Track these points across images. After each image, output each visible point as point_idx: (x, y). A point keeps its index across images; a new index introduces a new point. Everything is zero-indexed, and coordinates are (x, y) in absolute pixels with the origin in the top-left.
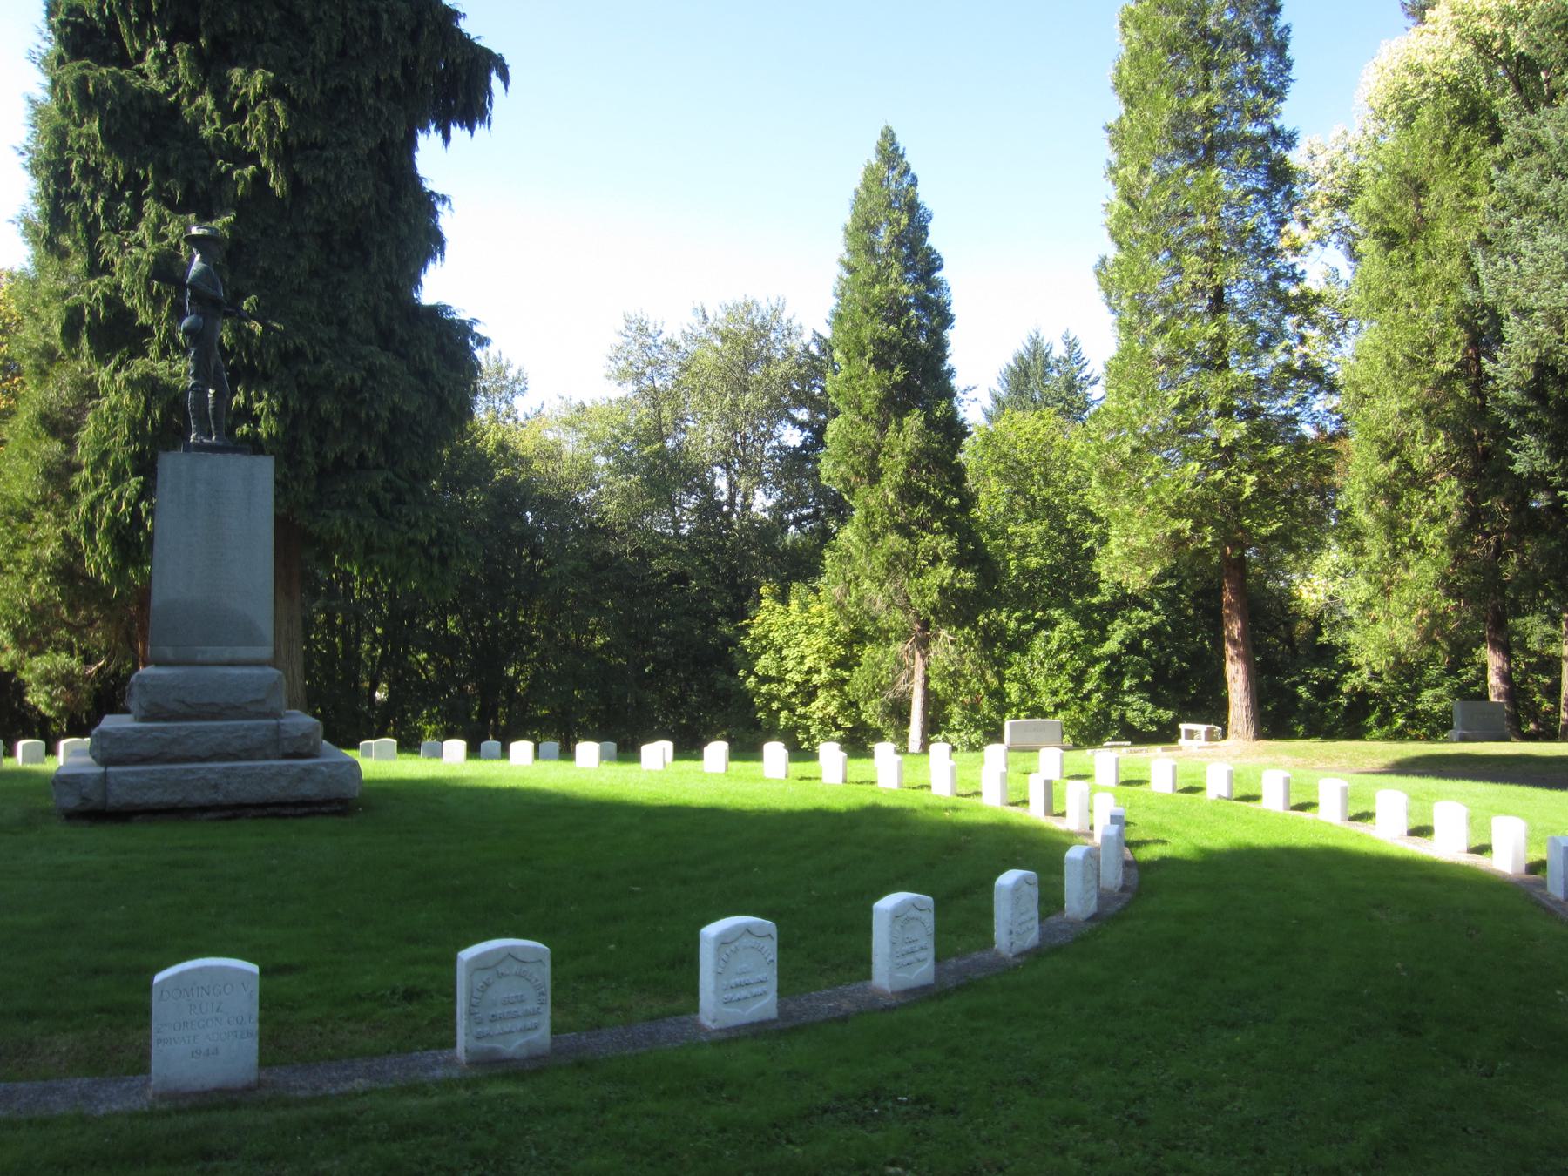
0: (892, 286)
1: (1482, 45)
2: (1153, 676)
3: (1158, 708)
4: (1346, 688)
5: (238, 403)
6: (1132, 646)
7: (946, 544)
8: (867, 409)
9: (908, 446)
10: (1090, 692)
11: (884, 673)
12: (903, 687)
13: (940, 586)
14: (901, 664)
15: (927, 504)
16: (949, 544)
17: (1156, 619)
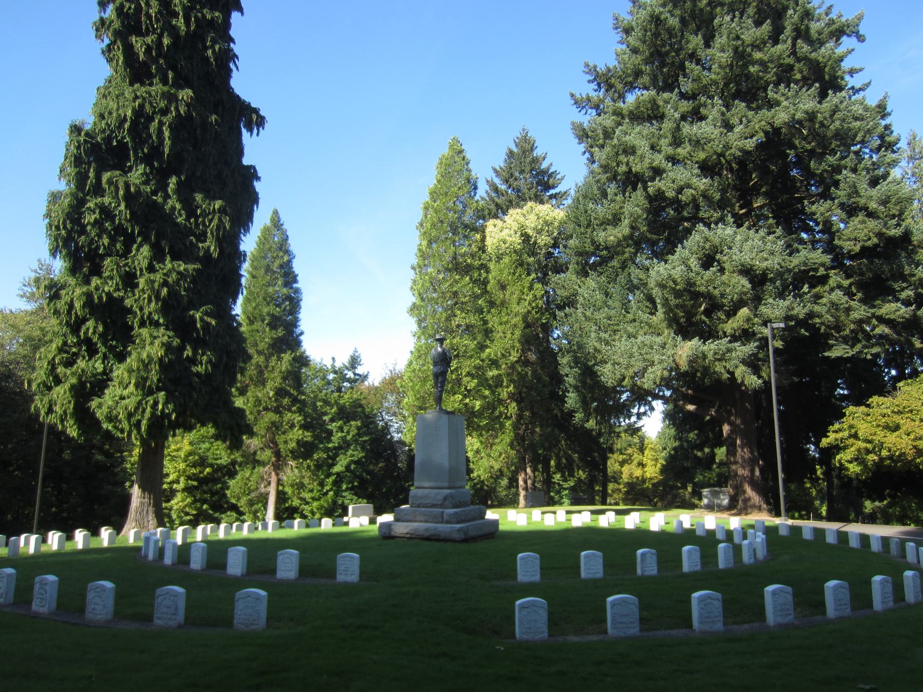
0: (277, 289)
1: (526, 238)
2: (358, 482)
5: (188, 355)
6: (348, 468)
7: (298, 418)
8: (260, 348)
9: (284, 369)
10: (328, 491)
11: (252, 483)
12: (263, 490)
14: (262, 478)
15: (290, 398)
16: (300, 418)
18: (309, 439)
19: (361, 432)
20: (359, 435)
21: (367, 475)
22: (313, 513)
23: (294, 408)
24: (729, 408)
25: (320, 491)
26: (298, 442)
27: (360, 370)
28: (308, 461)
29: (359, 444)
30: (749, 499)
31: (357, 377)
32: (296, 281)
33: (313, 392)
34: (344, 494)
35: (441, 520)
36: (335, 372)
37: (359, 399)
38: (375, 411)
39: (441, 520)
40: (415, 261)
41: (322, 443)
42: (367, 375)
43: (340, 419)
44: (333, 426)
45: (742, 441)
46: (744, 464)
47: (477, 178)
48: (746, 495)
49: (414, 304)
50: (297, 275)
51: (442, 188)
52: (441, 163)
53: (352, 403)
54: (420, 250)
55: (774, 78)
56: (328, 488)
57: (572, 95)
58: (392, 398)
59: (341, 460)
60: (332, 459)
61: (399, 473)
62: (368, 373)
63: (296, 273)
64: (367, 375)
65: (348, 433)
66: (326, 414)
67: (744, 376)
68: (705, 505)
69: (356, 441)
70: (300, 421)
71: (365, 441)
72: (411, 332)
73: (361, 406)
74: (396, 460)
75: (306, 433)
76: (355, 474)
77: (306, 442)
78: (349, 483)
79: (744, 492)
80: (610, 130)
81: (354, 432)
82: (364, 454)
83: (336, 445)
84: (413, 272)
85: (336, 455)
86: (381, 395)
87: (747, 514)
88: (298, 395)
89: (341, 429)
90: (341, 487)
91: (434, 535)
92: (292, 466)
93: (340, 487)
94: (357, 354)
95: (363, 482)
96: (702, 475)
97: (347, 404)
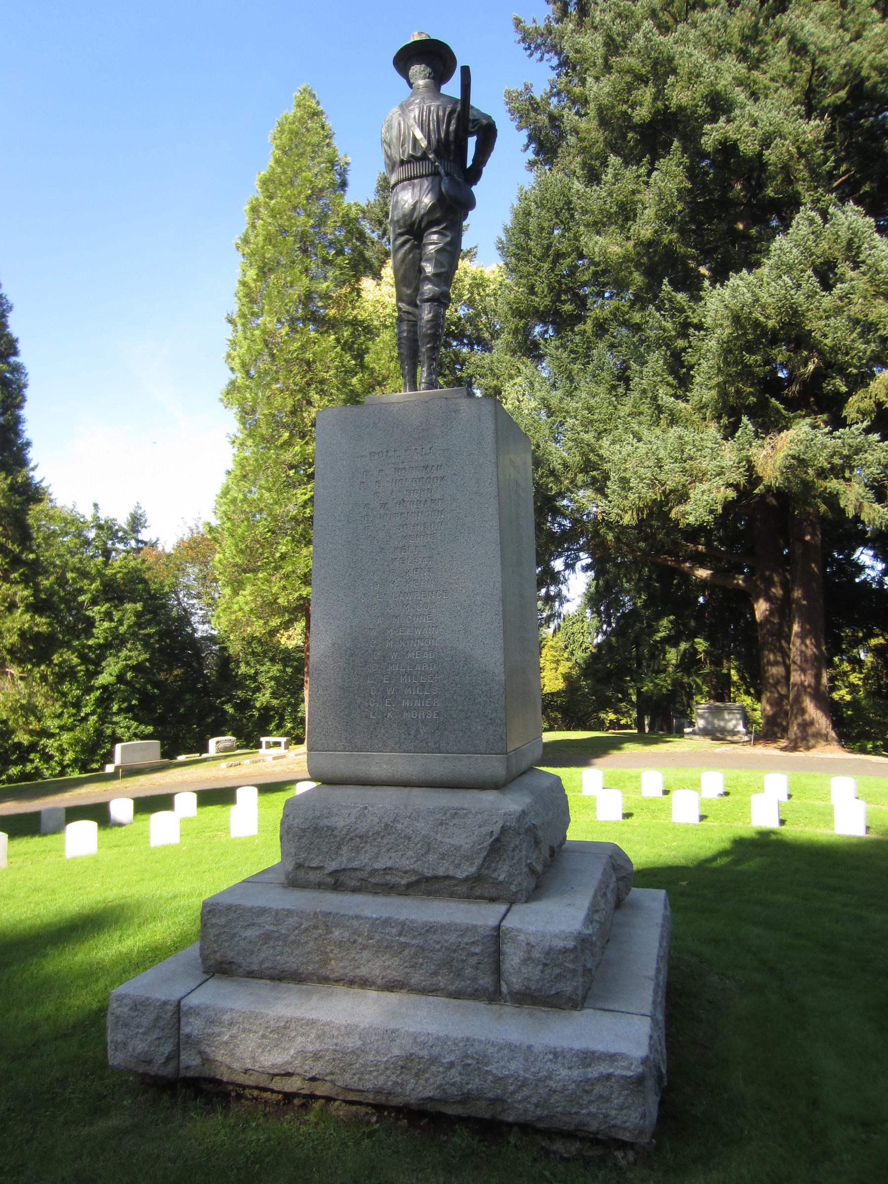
2: (138, 699)
3: (140, 724)
4: (258, 705)
6: (120, 678)
10: (87, 715)
13: (20, 629)
16: (26, 593)
17: (142, 658)
18: (44, 629)
19: (143, 620)
20: (139, 625)
21: (153, 688)
22: (63, 752)
23: (15, 576)
24: (767, 573)
25: (74, 715)
26: (22, 634)
27: (144, 535)
28: (43, 667)
29: (139, 640)
30: (812, 723)
31: (140, 545)
32: (16, 353)
33: (60, 556)
34: (115, 719)
35: (485, 981)
36: (100, 527)
37: (140, 570)
38: (167, 589)
39: (485, 981)
40: (234, 307)
41: (78, 638)
42: (156, 543)
43: (107, 600)
44: (95, 612)
45: (802, 627)
46: (804, 665)
47: (347, 164)
48: (807, 717)
49: (233, 383)
50: (17, 340)
51: (284, 173)
52: (282, 132)
53: (127, 574)
54: (244, 284)
55: (203, 655)
56: (88, 710)
57: (518, 22)
58: (193, 571)
59: (109, 665)
60: (94, 665)
61: (205, 684)
62: (158, 540)
63: (15, 335)
64: (156, 543)
65: (120, 622)
66: (81, 591)
67: (861, 505)
68: (700, 729)
69: (134, 635)
70: (27, 598)
71: (149, 636)
72: (228, 435)
73: (144, 581)
74: (200, 664)
75: (38, 619)
76: (133, 687)
77: (39, 634)
78: (123, 702)
79: (803, 711)
80: (619, 39)
81: (129, 619)
82: (147, 656)
83: (102, 641)
84: (230, 327)
85: (102, 657)
86: (175, 564)
87: (808, 748)
88: (21, 552)
89: (108, 616)
90: (111, 709)
91: (466, 1099)
92: (12, 675)
93: (108, 708)
94: (140, 512)
95: (147, 701)
96: (652, 682)
97: (119, 576)
